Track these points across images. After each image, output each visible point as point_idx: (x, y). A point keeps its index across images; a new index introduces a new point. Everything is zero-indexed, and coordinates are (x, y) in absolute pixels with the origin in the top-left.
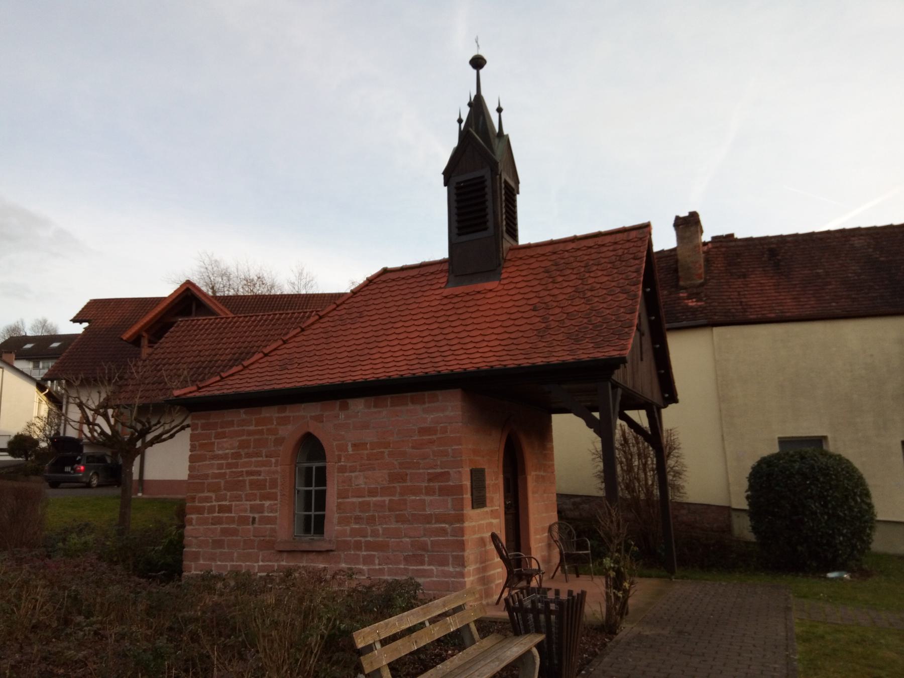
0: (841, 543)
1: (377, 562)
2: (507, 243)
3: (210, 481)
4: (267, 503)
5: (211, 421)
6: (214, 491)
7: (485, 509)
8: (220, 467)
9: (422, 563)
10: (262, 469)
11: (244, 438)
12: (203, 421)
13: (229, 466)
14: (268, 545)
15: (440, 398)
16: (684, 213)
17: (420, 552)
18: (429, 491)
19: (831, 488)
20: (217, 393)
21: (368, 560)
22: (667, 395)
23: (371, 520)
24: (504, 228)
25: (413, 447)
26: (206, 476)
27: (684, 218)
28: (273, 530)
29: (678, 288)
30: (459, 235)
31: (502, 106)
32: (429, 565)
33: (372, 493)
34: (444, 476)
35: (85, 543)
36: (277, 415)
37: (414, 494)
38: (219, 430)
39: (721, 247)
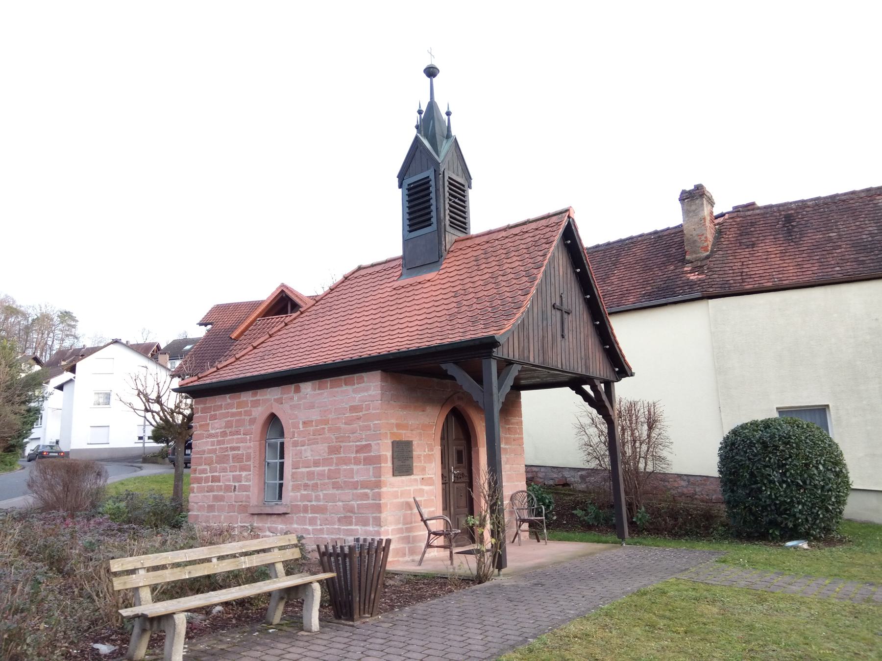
0: (801, 512)
1: (319, 522)
2: (451, 236)
3: (206, 455)
4: (244, 474)
5: (208, 405)
6: (209, 464)
7: (412, 477)
8: (213, 444)
9: (351, 524)
10: (241, 445)
11: (229, 419)
12: (202, 406)
13: (219, 443)
14: (243, 509)
15: (365, 379)
16: (690, 187)
17: (349, 514)
18: (357, 462)
19: (791, 457)
20: (214, 380)
21: (312, 521)
22: (617, 369)
23: (315, 487)
24: (448, 223)
25: (346, 424)
26: (204, 452)
27: (690, 192)
28: (248, 497)
29: (684, 262)
30: (410, 231)
31: (451, 110)
32: (356, 525)
33: (316, 463)
34: (367, 447)
35: (118, 507)
36: (251, 399)
37: (346, 464)
38: (213, 413)
39: (738, 217)
